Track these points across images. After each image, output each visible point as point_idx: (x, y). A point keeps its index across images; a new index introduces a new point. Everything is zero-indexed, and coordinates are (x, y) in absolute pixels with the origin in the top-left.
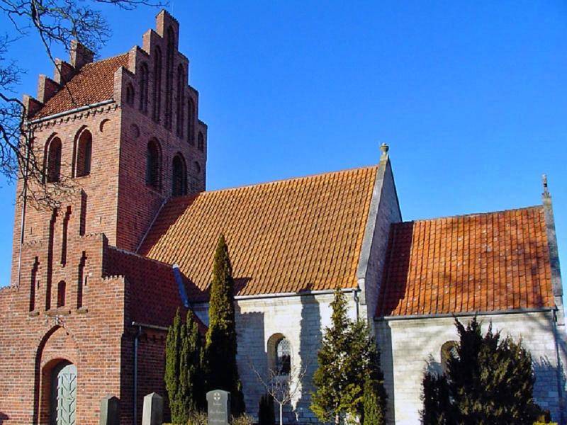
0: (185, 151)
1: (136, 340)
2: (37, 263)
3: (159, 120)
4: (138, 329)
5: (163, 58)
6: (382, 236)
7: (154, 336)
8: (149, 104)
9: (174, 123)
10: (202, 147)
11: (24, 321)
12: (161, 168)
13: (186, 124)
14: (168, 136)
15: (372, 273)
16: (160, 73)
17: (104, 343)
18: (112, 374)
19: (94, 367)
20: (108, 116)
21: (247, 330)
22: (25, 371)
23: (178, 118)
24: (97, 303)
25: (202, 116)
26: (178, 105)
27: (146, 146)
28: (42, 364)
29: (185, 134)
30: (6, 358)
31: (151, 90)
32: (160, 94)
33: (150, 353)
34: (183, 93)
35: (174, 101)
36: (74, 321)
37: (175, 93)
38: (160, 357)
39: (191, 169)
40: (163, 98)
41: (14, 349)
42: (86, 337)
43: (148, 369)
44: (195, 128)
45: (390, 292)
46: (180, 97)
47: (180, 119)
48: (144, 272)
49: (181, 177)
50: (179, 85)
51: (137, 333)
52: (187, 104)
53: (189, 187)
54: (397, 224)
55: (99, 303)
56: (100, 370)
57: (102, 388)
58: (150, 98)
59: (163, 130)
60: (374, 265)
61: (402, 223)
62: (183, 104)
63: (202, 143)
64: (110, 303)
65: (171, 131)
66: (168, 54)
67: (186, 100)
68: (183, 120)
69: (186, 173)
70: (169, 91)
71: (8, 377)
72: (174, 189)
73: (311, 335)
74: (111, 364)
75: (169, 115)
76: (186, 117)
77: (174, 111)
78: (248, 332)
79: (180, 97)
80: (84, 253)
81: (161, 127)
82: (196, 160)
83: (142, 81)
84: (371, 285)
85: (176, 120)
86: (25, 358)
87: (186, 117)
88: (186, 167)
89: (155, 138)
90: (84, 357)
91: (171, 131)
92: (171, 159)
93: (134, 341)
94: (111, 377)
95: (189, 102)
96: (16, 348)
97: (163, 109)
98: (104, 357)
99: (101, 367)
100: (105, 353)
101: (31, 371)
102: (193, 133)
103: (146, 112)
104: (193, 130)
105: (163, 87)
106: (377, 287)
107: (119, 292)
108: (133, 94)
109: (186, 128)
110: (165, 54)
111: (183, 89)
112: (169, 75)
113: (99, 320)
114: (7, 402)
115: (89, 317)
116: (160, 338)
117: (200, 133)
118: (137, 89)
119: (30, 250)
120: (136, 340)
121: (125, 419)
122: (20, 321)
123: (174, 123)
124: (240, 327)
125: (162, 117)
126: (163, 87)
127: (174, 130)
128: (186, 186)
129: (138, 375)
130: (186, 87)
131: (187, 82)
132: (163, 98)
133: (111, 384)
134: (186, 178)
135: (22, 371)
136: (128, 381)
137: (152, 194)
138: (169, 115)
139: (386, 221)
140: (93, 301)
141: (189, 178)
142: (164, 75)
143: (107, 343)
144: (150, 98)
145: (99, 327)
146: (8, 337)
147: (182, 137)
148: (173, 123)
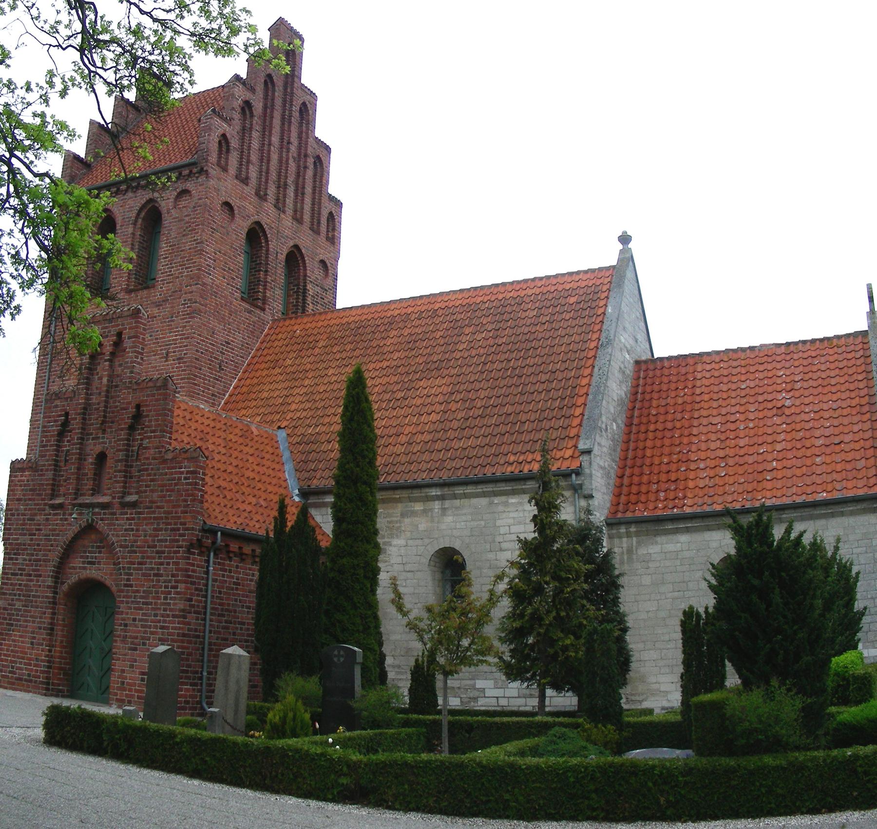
0: (306, 241)
1: (212, 554)
2: (65, 424)
3: (247, 178)
4: (216, 535)
5: (276, 94)
6: (620, 382)
7: (240, 548)
8: (251, 167)
9: (290, 201)
10: (333, 239)
11: (41, 514)
12: (266, 271)
13: (308, 200)
14: (279, 220)
15: (603, 444)
16: (272, 117)
17: (160, 558)
18: (171, 610)
19: (142, 597)
20: (189, 185)
21: (395, 542)
22: (39, 597)
23: (296, 191)
24: (152, 491)
25: (334, 189)
26: (298, 167)
27: (244, 236)
28: (65, 587)
29: (307, 217)
30: (12, 574)
31: (255, 145)
32: (269, 151)
33: (233, 577)
34: (306, 150)
35: (291, 161)
36: (117, 519)
37: (293, 149)
38: (248, 585)
39: (313, 271)
40: (275, 157)
41: (25, 560)
42: (132, 546)
43: (229, 605)
44: (323, 208)
45: (631, 485)
46: (302, 155)
47: (299, 191)
48: (230, 440)
49: (298, 285)
50: (300, 137)
51: (214, 543)
52: (311, 167)
53: (309, 299)
54: (646, 362)
55: (156, 491)
56: (151, 603)
57: (152, 633)
58: (254, 158)
59: (272, 210)
60: (606, 430)
61: (653, 361)
62: (306, 167)
63: (334, 230)
64: (172, 491)
65: (284, 212)
66: (285, 89)
67: (310, 161)
68: (303, 194)
69: (305, 279)
70: (284, 144)
71: (14, 605)
72: (287, 304)
73: (501, 550)
74: (170, 593)
75: (282, 186)
76: (308, 190)
77: (290, 180)
78: (395, 546)
79: (302, 155)
80: (138, 407)
81: (269, 207)
82: (321, 257)
83: (244, 129)
84: (602, 464)
85: (292, 195)
86: (40, 576)
87: (308, 190)
88: (305, 269)
89: (258, 223)
90: (128, 580)
91: (284, 212)
92: (282, 257)
93: (209, 557)
94: (168, 616)
95: (315, 163)
96: (27, 558)
97: (273, 175)
98: (158, 581)
99: (154, 598)
100: (161, 575)
101: (47, 597)
102: (319, 214)
103: (245, 181)
104: (320, 208)
105: (275, 139)
106: (613, 468)
107: (188, 472)
108: (228, 151)
109: (307, 207)
110: (281, 88)
111: (307, 144)
112: (286, 120)
113: (155, 518)
114: (10, 646)
115: (140, 513)
116: (250, 552)
117: (331, 214)
118: (234, 143)
119: (58, 402)
120: (212, 554)
121: (187, 690)
122: (36, 515)
123: (290, 201)
124: (383, 537)
125: (272, 190)
126: (275, 139)
127: (290, 211)
128: (304, 300)
129: (211, 614)
130: (311, 140)
131: (313, 131)
132: (275, 157)
133: (167, 628)
134: (305, 286)
135: (34, 596)
136: (196, 624)
137: (250, 312)
138: (282, 186)
139: (627, 356)
140: (146, 486)
141: (309, 286)
142: (277, 122)
143: (165, 558)
144: (254, 158)
145: (155, 530)
146: (17, 539)
147: (317, 232)
148: (287, 200)
